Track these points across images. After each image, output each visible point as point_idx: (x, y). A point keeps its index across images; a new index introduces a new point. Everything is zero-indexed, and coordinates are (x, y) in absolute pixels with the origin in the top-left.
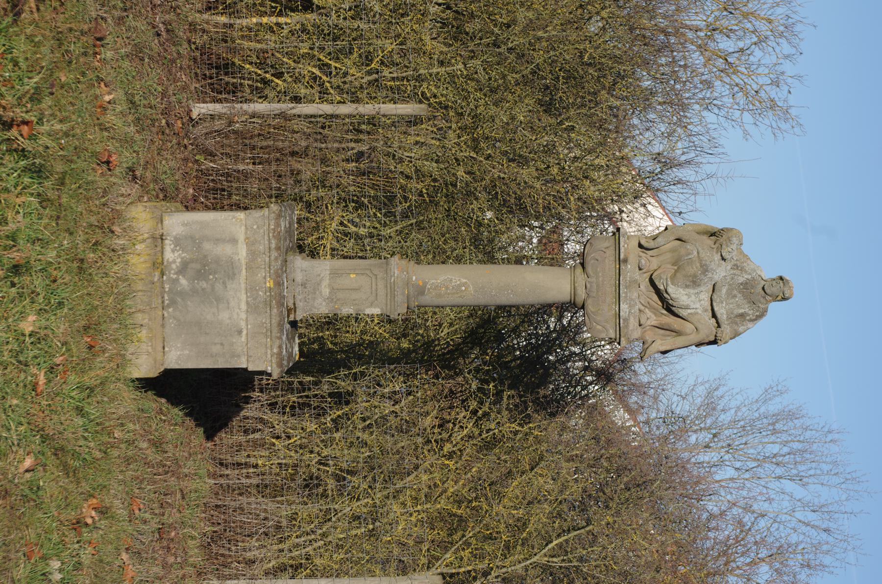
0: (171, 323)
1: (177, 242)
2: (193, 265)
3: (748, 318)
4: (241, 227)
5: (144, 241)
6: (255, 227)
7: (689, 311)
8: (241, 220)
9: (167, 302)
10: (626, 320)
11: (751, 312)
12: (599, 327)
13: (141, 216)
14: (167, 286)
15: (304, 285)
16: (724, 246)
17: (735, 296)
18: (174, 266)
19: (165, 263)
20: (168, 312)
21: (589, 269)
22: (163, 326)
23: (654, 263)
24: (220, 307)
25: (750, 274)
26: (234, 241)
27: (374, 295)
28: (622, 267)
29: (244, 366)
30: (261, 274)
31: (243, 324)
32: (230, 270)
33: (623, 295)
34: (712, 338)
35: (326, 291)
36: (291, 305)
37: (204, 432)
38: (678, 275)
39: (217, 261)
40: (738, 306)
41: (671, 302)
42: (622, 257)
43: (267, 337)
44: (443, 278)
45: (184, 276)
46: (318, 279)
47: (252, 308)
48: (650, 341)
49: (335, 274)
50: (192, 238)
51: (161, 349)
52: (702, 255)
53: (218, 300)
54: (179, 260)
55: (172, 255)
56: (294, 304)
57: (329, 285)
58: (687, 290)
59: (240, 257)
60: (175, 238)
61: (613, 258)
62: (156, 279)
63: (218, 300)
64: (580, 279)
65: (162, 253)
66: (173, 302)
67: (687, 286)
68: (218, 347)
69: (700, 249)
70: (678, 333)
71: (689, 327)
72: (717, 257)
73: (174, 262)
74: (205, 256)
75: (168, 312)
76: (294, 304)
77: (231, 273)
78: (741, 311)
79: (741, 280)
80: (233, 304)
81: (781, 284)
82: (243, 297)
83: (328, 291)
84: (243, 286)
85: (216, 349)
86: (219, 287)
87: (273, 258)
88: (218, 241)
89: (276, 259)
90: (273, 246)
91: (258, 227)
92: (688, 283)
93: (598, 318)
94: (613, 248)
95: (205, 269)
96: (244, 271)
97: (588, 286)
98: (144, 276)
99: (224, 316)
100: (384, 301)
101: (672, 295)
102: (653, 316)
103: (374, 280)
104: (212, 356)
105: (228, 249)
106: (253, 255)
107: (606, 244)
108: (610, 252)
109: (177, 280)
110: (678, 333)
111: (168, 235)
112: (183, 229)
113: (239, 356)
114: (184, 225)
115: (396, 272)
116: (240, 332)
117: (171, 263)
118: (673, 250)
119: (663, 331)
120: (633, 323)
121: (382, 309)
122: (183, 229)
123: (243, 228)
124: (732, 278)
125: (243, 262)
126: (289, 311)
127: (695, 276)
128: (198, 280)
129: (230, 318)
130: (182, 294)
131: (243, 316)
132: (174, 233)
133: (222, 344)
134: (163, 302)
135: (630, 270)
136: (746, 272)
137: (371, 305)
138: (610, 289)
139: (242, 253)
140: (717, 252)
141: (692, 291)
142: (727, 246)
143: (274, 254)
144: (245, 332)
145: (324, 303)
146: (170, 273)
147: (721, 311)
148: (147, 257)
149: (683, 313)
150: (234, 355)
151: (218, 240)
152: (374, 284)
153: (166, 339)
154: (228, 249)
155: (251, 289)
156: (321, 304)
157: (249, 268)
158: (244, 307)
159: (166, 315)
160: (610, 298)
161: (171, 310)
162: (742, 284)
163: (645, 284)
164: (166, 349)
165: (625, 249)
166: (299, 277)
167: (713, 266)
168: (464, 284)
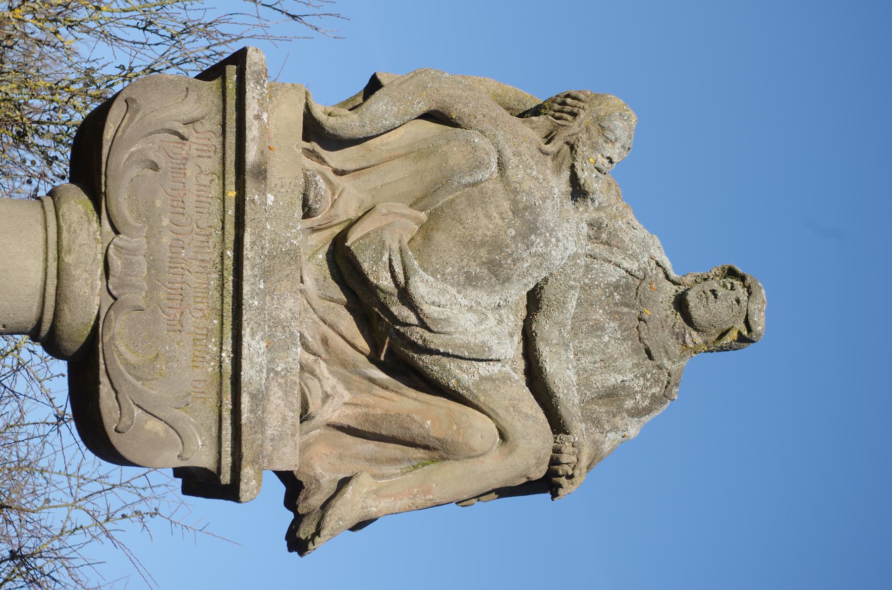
3: (629, 404)
7: (484, 369)
10: (259, 398)
11: (638, 385)
12: (154, 426)
16: (581, 149)
17: (597, 328)
21: (120, 197)
23: (348, 200)
25: (634, 257)
28: (252, 192)
33: (250, 300)
34: (538, 473)
37: (205, 470)
38: (439, 237)
40: (608, 363)
41: (417, 334)
42: (251, 155)
48: (328, 480)
58: (473, 293)
61: (212, 164)
67: (471, 281)
69: (508, 153)
70: (435, 450)
71: (479, 429)
72: (561, 185)
78: (613, 379)
79: (614, 275)
81: (741, 292)
92: (475, 269)
93: (153, 391)
94: (212, 124)
97: (116, 263)
101: (427, 309)
102: (341, 388)
107: (190, 108)
108: (205, 141)
110: (435, 450)
118: (418, 152)
119: (371, 447)
120: (280, 410)
124: (588, 268)
127: (496, 244)
135: (273, 203)
136: (624, 250)
138: (202, 283)
140: (558, 170)
141: (486, 299)
147: (560, 370)
149: (461, 375)
160: (202, 314)
162: (617, 287)
163: (315, 271)
165: (264, 131)
167: (549, 215)
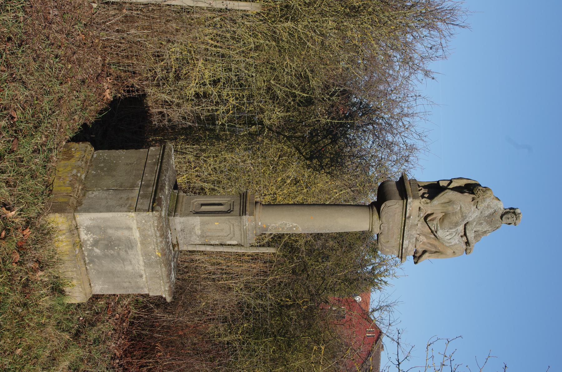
0: (92, 273)
1: (89, 229)
2: (103, 242)
4: (133, 221)
5: (64, 234)
6: (143, 221)
8: (133, 217)
9: (87, 261)
13: (58, 221)
14: (86, 254)
15: (182, 230)
18: (89, 242)
19: (82, 241)
20: (90, 267)
22: (88, 274)
24: (125, 263)
26: (129, 228)
27: (232, 233)
28: (407, 221)
29: (147, 293)
30: (151, 248)
31: (143, 272)
32: (130, 245)
35: (199, 232)
36: (175, 242)
39: (119, 239)
42: (407, 215)
43: (160, 280)
44: (279, 223)
45: (97, 248)
46: (192, 226)
47: (148, 264)
49: (203, 224)
50: (99, 227)
51: (88, 286)
52: (463, 209)
53: (124, 260)
54: (92, 239)
55: (86, 236)
56: (177, 242)
57: (200, 229)
59: (135, 237)
60: (86, 227)
61: (401, 213)
62: (77, 252)
63: (124, 260)
64: (376, 224)
65: (79, 235)
66: (92, 261)
68: (128, 283)
69: (462, 205)
73: (88, 240)
74: (110, 237)
75: (90, 267)
76: (177, 242)
77: (130, 246)
80: (133, 262)
82: (141, 258)
83: (200, 232)
84: (140, 252)
85: (126, 285)
86: (122, 253)
87: (158, 241)
88: (117, 229)
89: (161, 242)
90: (158, 235)
91: (145, 221)
95: (111, 245)
96: (139, 245)
98: (68, 253)
99: (129, 268)
100: (240, 238)
103: (231, 226)
104: (124, 288)
105: (126, 233)
106: (144, 238)
109: (93, 250)
111: (81, 225)
112: (91, 222)
113: (142, 288)
114: (91, 219)
115: (247, 224)
116: (141, 276)
117: (86, 241)
121: (238, 242)
122: (91, 222)
123: (135, 221)
125: (138, 240)
126: (174, 246)
128: (107, 249)
129: (133, 269)
130: (97, 257)
131: (143, 268)
132: (85, 225)
133: (129, 282)
134: (85, 261)
137: (231, 239)
139: (136, 235)
142: (482, 203)
143: (160, 239)
144: (144, 276)
145: (198, 239)
146: (86, 246)
148: (68, 243)
150: (138, 288)
151: (117, 228)
152: (232, 228)
153: (91, 280)
154: (126, 233)
155: (146, 255)
156: (196, 239)
157: (142, 244)
158: (142, 263)
159: (88, 268)
161: (91, 265)
164: (92, 285)
166: (179, 227)
168: (295, 227)
